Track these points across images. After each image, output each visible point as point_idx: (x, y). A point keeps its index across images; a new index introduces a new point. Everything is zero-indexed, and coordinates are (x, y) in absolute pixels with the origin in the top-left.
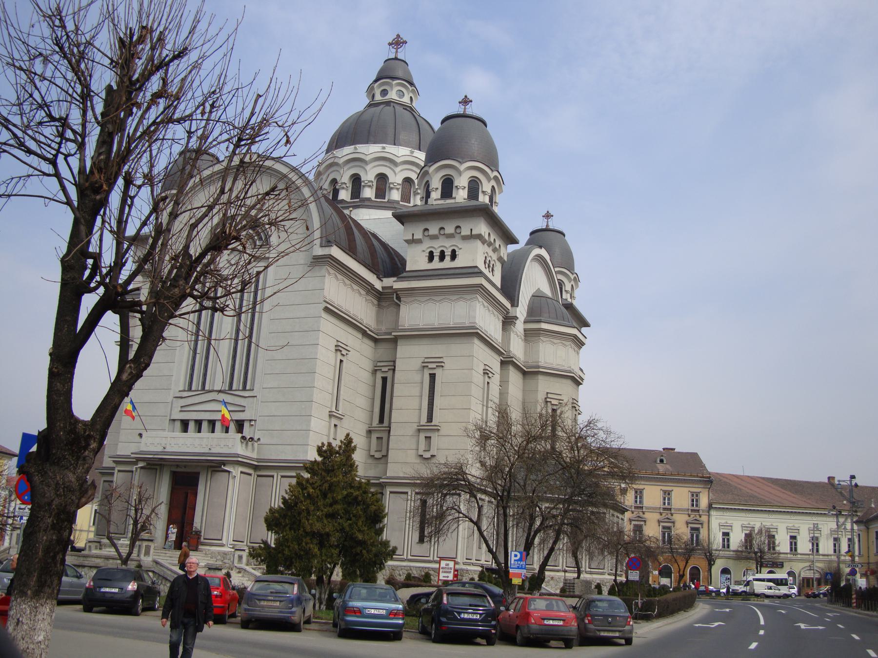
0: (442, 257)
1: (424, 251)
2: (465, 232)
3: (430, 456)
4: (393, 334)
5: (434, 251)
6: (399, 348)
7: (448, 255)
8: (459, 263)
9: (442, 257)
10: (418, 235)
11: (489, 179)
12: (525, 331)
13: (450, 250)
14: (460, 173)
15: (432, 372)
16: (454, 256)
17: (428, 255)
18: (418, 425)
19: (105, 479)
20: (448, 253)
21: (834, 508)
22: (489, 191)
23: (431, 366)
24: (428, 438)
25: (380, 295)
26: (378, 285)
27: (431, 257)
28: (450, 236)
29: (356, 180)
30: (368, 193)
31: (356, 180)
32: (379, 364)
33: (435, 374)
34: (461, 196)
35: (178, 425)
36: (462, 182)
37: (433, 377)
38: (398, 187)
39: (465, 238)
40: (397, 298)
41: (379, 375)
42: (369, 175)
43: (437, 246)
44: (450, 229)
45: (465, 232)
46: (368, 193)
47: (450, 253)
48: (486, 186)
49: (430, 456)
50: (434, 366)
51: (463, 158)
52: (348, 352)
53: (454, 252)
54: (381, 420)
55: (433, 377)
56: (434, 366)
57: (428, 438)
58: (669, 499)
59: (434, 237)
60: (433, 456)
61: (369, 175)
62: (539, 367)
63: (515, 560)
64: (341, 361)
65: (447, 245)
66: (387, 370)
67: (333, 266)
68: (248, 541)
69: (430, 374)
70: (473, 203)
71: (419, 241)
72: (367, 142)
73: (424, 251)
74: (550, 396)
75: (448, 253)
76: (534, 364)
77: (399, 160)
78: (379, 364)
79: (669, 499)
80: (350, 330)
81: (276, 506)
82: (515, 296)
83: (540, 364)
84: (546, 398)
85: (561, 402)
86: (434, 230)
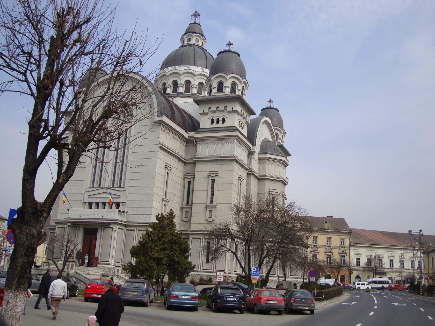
0: (218, 122)
1: (209, 119)
2: (229, 109)
3: (212, 220)
4: (194, 160)
5: (219, 118)
6: (196, 166)
7: (215, 121)
8: (226, 124)
9: (218, 122)
10: (206, 111)
11: (241, 83)
12: (259, 158)
13: (222, 118)
14: (227, 80)
15: (213, 178)
16: (224, 121)
17: (211, 120)
18: (206, 205)
19: (51, 232)
20: (221, 119)
21: (412, 246)
22: (241, 89)
23: (212, 175)
24: (211, 211)
25: (187, 140)
26: (186, 135)
27: (212, 122)
28: (222, 111)
29: (175, 83)
30: (181, 90)
31: (175, 83)
32: (186, 175)
33: (214, 180)
34: (227, 91)
35: (87, 205)
36: (228, 84)
37: (213, 181)
38: (196, 87)
39: (229, 112)
40: (195, 142)
41: (210, 179)
42: (182, 81)
43: (215, 116)
44: (222, 107)
45: (229, 109)
46: (181, 90)
47: (216, 120)
48: (240, 86)
49: (212, 220)
50: (214, 175)
51: (228, 73)
52: (171, 169)
53: (224, 119)
54: (188, 202)
55: (213, 181)
56: (214, 175)
57: (211, 211)
58: (330, 242)
59: (214, 112)
60: (213, 220)
61: (182, 81)
62: (266, 176)
63: (254, 272)
64: (168, 173)
65: (220, 116)
66: (190, 178)
67: (164, 126)
68: (122, 262)
69: (212, 180)
70: (233, 95)
71: (206, 114)
72: (180, 64)
73: (209, 119)
74: (271, 190)
75: (221, 119)
76: (264, 175)
77: (196, 74)
78: (186, 175)
79: (330, 242)
80: (172, 158)
81: (136, 245)
82: (254, 141)
83: (266, 175)
84: (269, 192)
85: (277, 193)
86: (214, 108)
